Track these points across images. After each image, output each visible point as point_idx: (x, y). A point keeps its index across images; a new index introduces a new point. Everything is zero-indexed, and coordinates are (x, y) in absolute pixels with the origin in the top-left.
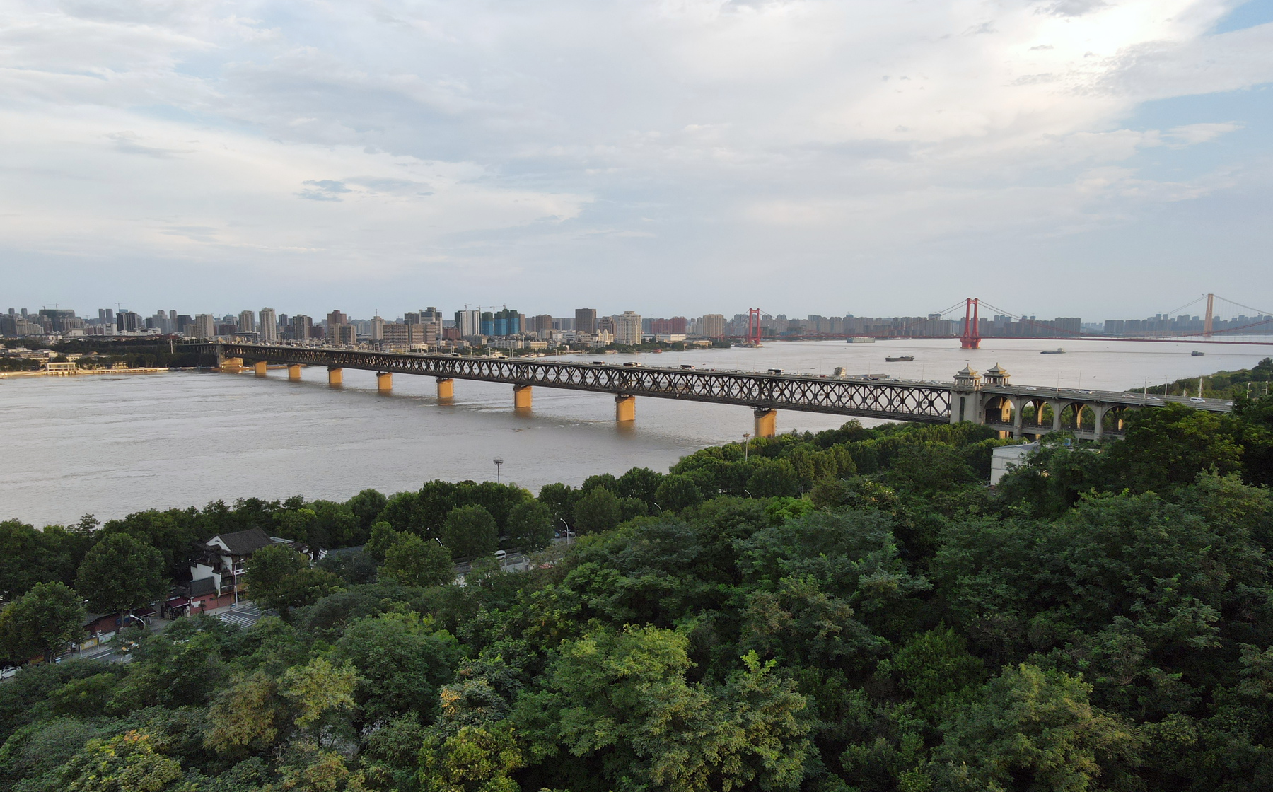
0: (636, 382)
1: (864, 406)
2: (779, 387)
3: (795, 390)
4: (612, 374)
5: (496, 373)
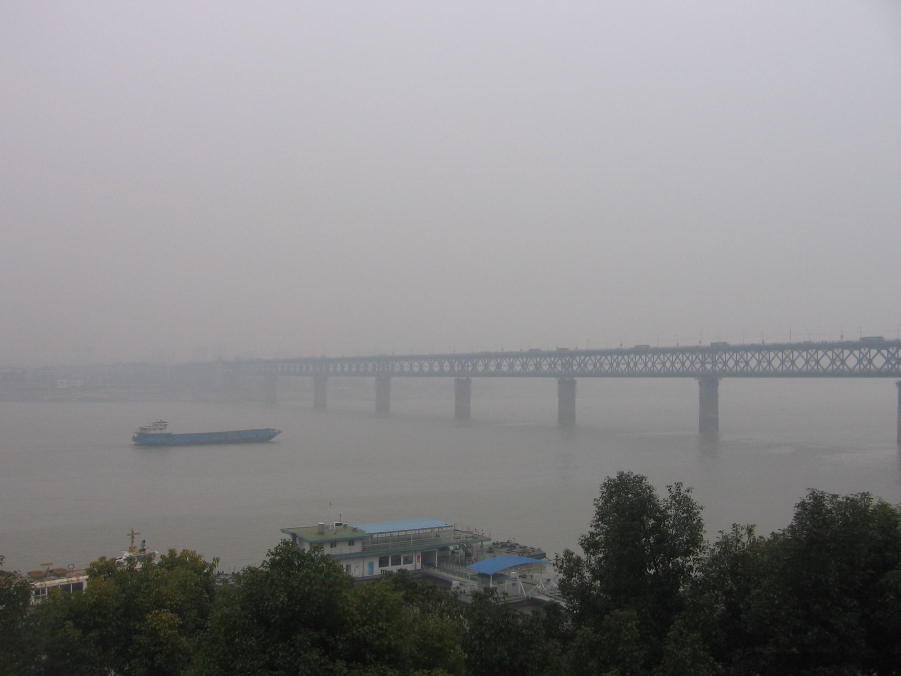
0: (577, 367)
1: (747, 367)
2: (625, 360)
3: (695, 360)
4: (513, 360)
5: (426, 369)
